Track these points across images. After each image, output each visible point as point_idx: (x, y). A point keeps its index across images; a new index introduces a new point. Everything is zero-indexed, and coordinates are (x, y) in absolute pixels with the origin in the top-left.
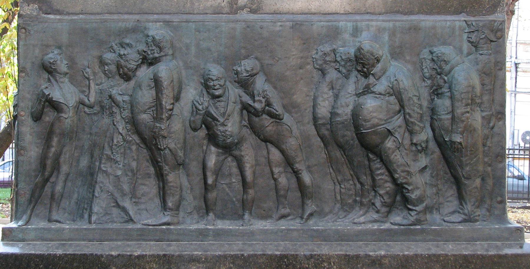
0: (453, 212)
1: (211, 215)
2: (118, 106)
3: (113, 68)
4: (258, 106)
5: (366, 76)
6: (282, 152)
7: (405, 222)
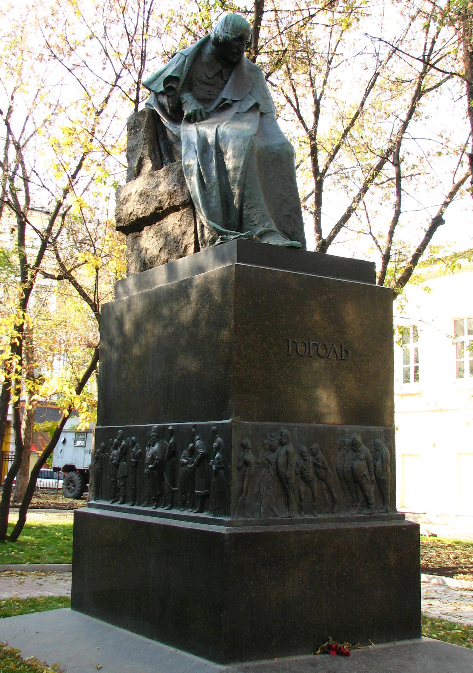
0: (381, 509)
1: (303, 513)
2: (271, 464)
3: (267, 446)
4: (320, 464)
5: (356, 451)
6: (326, 483)
7: (369, 513)
